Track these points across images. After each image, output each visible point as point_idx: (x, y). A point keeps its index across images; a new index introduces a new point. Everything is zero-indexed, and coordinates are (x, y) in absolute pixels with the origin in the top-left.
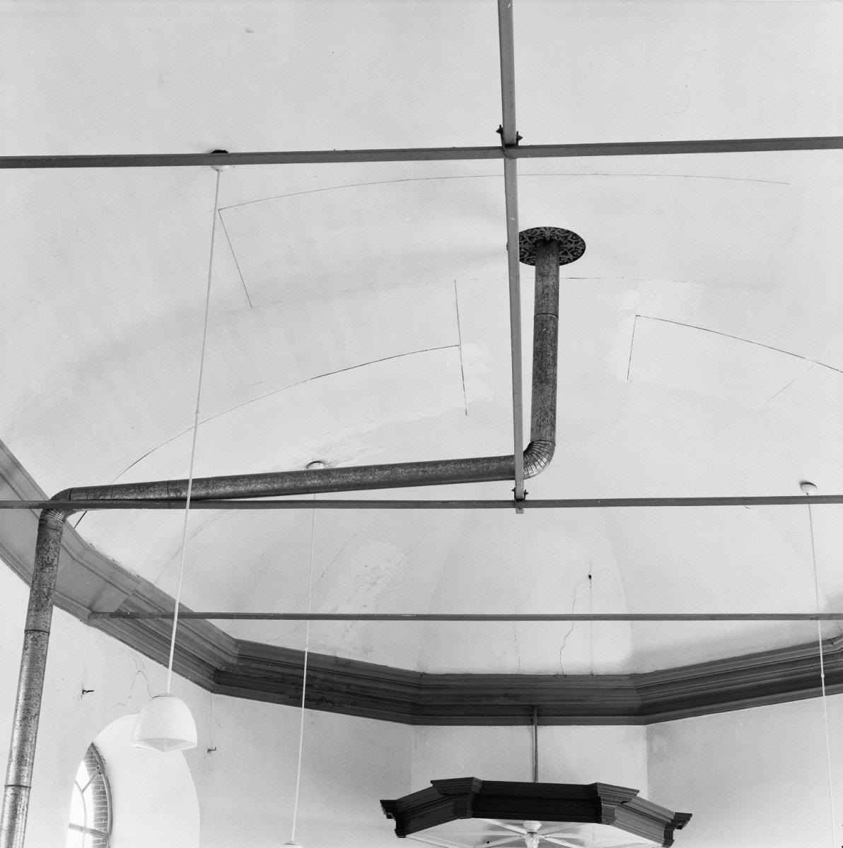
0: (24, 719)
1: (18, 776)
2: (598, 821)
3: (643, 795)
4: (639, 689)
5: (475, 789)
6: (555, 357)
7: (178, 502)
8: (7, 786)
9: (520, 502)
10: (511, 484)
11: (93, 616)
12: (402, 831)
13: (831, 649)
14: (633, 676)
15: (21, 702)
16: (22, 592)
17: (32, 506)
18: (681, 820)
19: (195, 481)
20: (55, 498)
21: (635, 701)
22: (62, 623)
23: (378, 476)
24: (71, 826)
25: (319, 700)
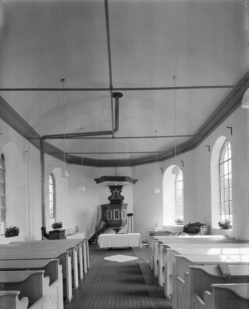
0: (42, 171)
1: (43, 180)
2: (125, 181)
3: (131, 177)
4: (131, 162)
5: (108, 177)
6: (118, 114)
7: (63, 138)
8: (41, 181)
9: (113, 138)
10: (112, 135)
11: (49, 153)
12: (97, 183)
13: (158, 156)
14: (130, 160)
15: (41, 169)
16: (39, 152)
17: (39, 139)
18: (136, 180)
19: (65, 134)
20: (42, 137)
21: (130, 163)
22: (46, 155)
23: (92, 134)
24: (50, 184)
25: (84, 164)
